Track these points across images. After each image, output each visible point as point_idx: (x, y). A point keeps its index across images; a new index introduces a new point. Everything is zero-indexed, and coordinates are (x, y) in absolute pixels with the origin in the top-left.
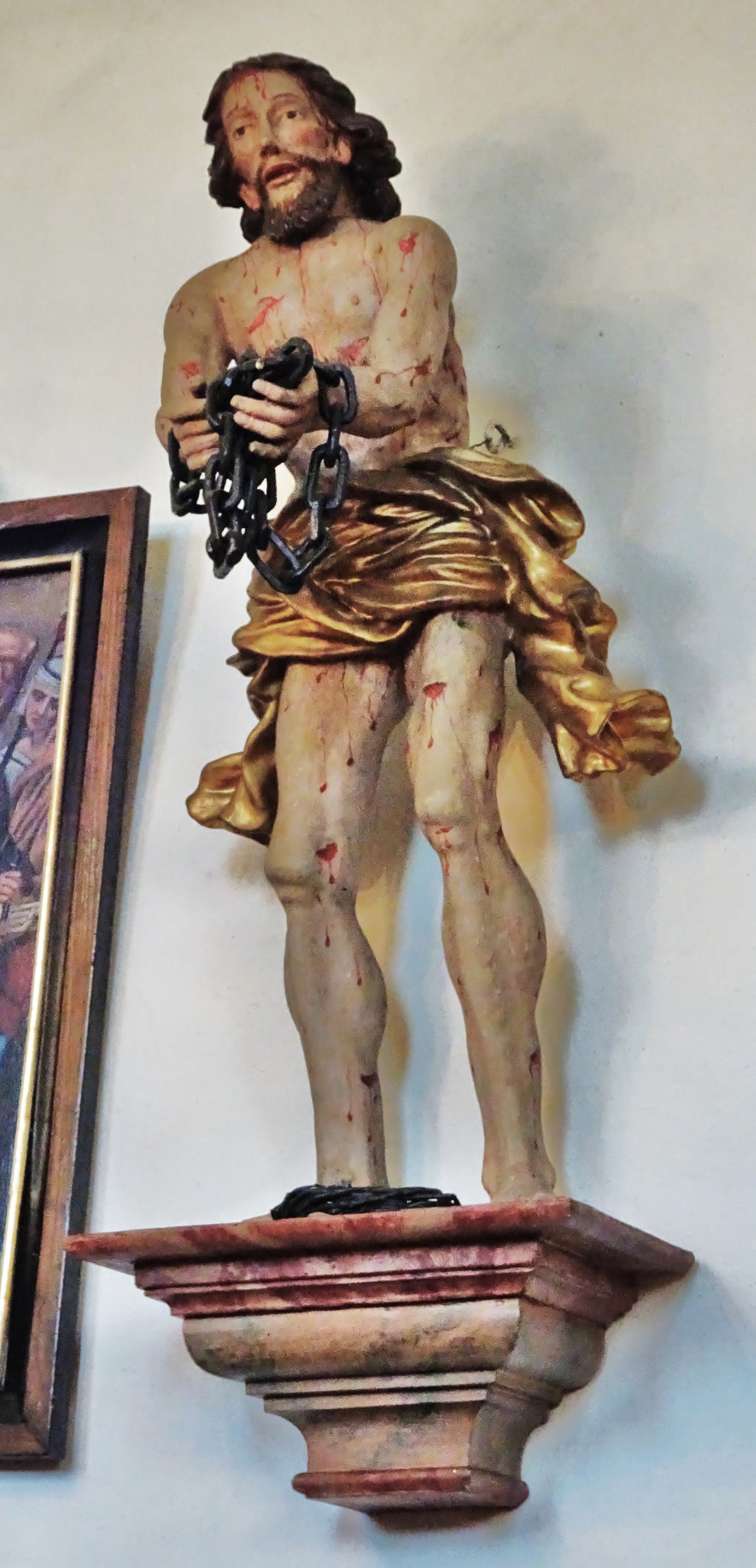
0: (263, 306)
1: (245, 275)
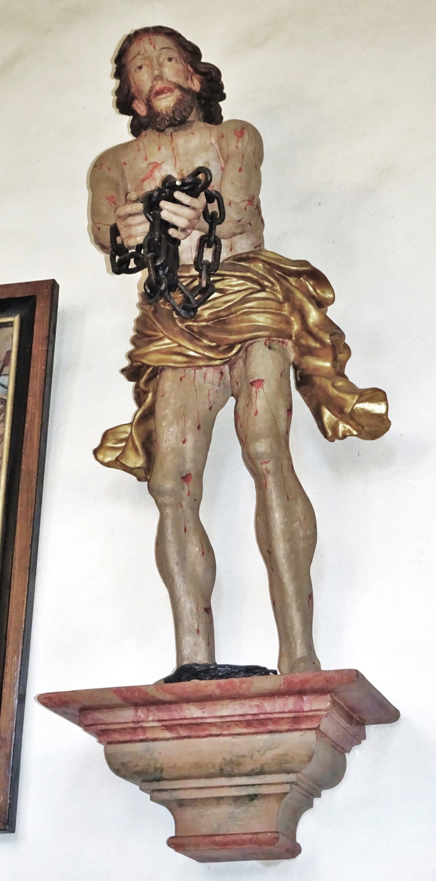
0: (151, 167)
1: (139, 150)
